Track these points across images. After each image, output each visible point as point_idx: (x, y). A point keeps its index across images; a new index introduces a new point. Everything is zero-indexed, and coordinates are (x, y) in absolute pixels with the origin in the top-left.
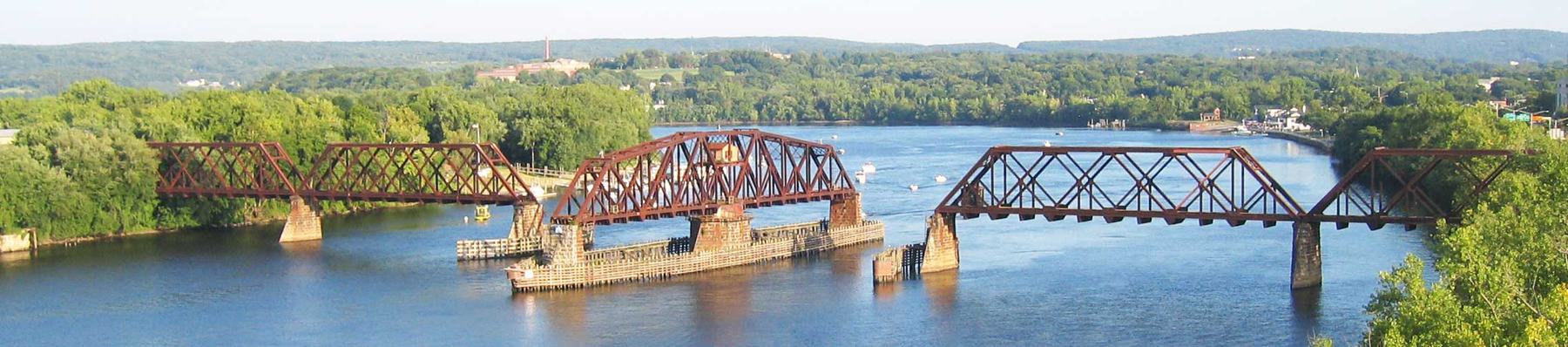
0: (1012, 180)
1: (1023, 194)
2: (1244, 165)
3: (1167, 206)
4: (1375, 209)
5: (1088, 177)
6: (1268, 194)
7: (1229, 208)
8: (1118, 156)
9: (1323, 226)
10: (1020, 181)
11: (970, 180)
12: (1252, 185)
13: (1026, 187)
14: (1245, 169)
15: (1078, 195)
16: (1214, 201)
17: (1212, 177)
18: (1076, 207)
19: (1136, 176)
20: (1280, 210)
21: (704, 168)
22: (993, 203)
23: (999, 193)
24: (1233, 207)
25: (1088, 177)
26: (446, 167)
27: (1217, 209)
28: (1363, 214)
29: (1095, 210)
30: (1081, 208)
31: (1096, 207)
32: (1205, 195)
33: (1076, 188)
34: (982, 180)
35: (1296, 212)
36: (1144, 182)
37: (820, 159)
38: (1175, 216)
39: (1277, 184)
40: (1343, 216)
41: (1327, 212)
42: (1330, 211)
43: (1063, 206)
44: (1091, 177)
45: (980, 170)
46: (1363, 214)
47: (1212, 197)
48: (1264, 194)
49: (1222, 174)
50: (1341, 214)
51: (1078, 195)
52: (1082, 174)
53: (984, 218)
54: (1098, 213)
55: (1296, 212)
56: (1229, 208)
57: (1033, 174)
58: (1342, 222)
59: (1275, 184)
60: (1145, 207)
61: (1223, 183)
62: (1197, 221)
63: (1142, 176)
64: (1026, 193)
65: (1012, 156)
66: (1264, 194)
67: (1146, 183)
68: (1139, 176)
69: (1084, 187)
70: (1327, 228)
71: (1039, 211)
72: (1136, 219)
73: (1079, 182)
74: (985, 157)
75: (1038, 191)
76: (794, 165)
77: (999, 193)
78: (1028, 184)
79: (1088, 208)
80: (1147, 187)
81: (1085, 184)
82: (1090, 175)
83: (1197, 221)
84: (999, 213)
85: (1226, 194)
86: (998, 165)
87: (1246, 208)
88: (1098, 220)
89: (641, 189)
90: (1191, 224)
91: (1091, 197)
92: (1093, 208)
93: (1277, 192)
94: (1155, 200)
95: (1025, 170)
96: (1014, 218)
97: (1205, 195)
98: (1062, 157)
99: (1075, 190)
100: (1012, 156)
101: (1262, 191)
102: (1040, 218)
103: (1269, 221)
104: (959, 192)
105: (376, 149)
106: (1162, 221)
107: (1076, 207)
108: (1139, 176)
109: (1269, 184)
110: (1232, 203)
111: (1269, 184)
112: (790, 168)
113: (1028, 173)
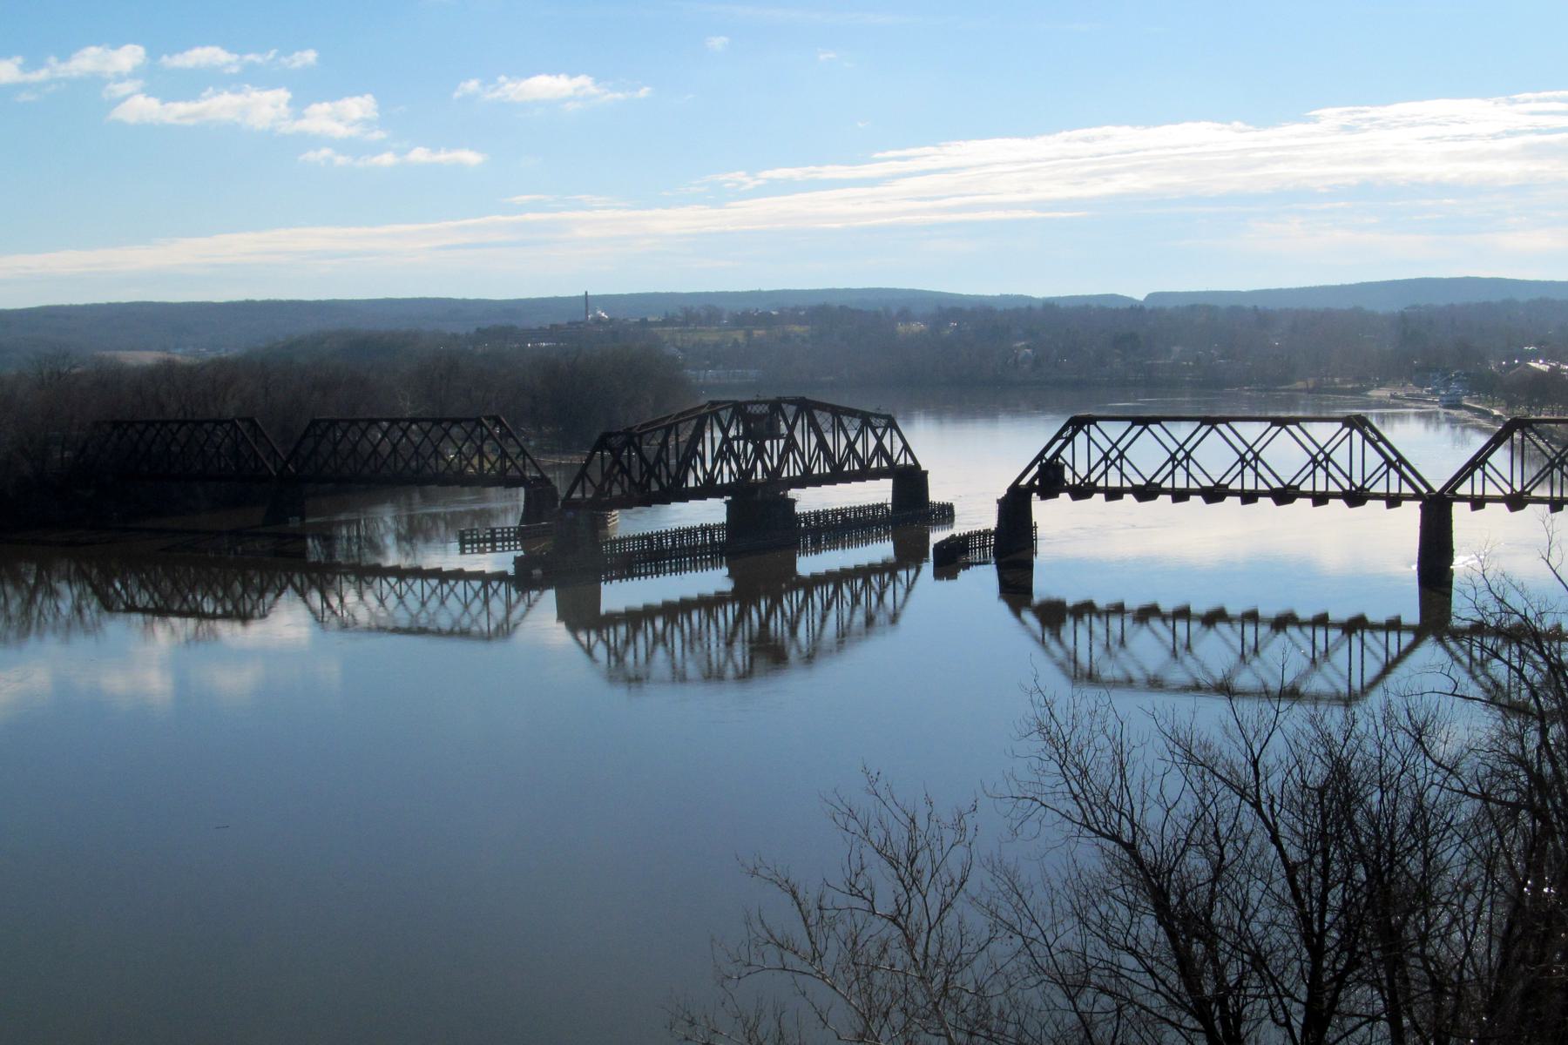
0: (1096, 456)
1: (1317, 470)
2: (1365, 437)
4: (1515, 486)
5: (1184, 450)
6: (1392, 470)
7: (1346, 485)
10: (1106, 457)
11: (1048, 455)
12: (1374, 459)
13: (1180, 463)
15: (1172, 472)
16: (1385, 476)
19: (1311, 451)
20: (1407, 489)
22: (622, 477)
23: (1082, 470)
24: (1352, 484)
25: (1184, 450)
26: (416, 439)
27: (1333, 488)
28: (1502, 494)
29: (1260, 491)
30: (1486, 494)
34: (1489, 460)
35: (1424, 491)
36: (1249, 456)
37: (879, 432)
38: (1285, 495)
39: (1039, 455)
40: (692, 488)
41: (1460, 491)
42: (1464, 489)
43: (1156, 484)
44: (1121, 449)
45: (1059, 443)
47: (1328, 475)
48: (1387, 472)
50: (1555, 495)
51: (1172, 472)
53: (1065, 497)
54: (1195, 492)
55: (1424, 491)
56: (1346, 485)
57: (1121, 446)
58: (1478, 503)
59: (1401, 459)
60: (1321, 488)
61: (1340, 456)
64: (1179, 470)
65: (1098, 427)
66: (1387, 472)
69: (1180, 463)
70: (1460, 511)
71: (1127, 491)
73: (1173, 457)
75: (1332, 468)
77: (1082, 470)
78: (1116, 459)
80: (1324, 463)
81: (1180, 458)
82: (1121, 446)
84: (1082, 491)
85: (1262, 465)
86: (1081, 438)
88: (1196, 500)
91: (1189, 474)
93: (1404, 468)
95: (1111, 442)
97: (1320, 472)
99: (1169, 467)
100: (1098, 427)
102: (1129, 498)
103: (1393, 501)
104: (1035, 469)
106: (1341, 503)
107: (1469, 492)
108: (1315, 451)
109: (1394, 458)
110: (1350, 479)
111: (1394, 458)
113: (1114, 446)
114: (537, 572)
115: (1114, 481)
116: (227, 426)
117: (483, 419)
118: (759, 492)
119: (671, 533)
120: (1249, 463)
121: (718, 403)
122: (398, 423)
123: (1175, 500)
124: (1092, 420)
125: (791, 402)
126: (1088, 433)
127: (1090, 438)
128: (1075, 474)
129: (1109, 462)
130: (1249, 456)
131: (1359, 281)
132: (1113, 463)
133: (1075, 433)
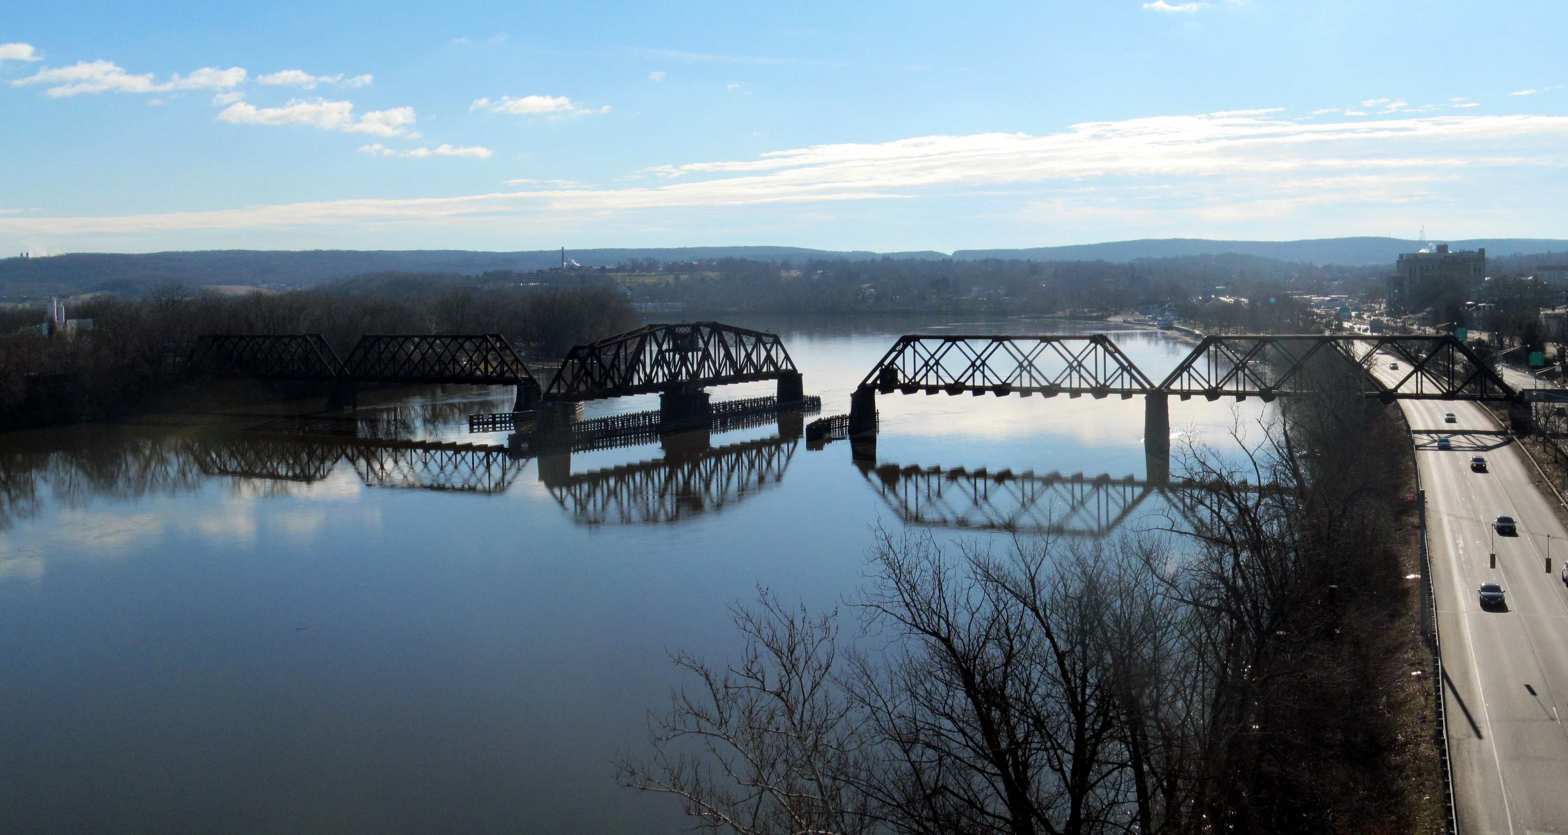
0: (920, 363)
1: (975, 374)
3: (1044, 383)
7: (1093, 383)
8: (1005, 342)
9: (1171, 398)
10: (926, 364)
14: (1107, 354)
17: (1080, 359)
18: (972, 384)
21: (671, 354)
23: (910, 373)
27: (1084, 385)
28: (1202, 389)
31: (987, 384)
32: (1025, 374)
33: (972, 368)
35: (1148, 387)
36: (1026, 364)
38: (1050, 391)
41: (1173, 387)
45: (894, 354)
46: (1202, 389)
48: (1122, 374)
49: (983, 350)
52: (976, 357)
53: (898, 392)
55: (1148, 387)
56: (1093, 383)
58: (1186, 395)
59: (1131, 365)
60: (1075, 385)
61: (1089, 363)
62: (1234, 397)
63: (1023, 358)
64: (931, 373)
66: (1122, 374)
67: (1075, 366)
68: (1071, 359)
70: (1173, 401)
71: (941, 388)
72: (1120, 395)
73: (973, 364)
74: (897, 344)
76: (746, 350)
77: (910, 373)
78: (933, 365)
79: (1029, 386)
80: (1078, 368)
81: (978, 365)
82: (983, 357)
83: (1234, 397)
84: (910, 388)
86: (909, 351)
87: (1108, 384)
89: (618, 370)
90: (1014, 395)
92: (939, 384)
93: (1133, 371)
94: (1205, 380)
96: (922, 393)
97: (1075, 375)
98: (1006, 343)
101: (1120, 371)
103: (1126, 394)
104: (877, 373)
105: (403, 339)
108: (1071, 359)
109: (1126, 364)
110: (1096, 379)
111: (1126, 364)
112: (743, 353)
114: (525, 446)
115: (932, 381)
116: (300, 340)
117: (307, 337)
118: (684, 388)
119: (621, 417)
120: (1025, 368)
121: (655, 326)
122: (426, 339)
123: (975, 394)
124: (916, 338)
125: (706, 325)
126: (914, 347)
127: (915, 351)
128: (905, 376)
129: (929, 368)
130: (1026, 364)
131: (330, 249)
132: (932, 368)
133: (905, 347)
